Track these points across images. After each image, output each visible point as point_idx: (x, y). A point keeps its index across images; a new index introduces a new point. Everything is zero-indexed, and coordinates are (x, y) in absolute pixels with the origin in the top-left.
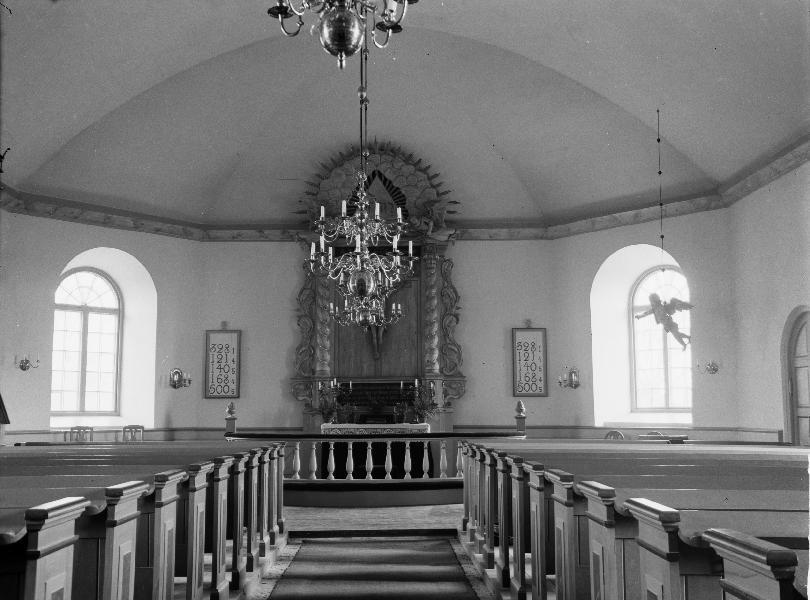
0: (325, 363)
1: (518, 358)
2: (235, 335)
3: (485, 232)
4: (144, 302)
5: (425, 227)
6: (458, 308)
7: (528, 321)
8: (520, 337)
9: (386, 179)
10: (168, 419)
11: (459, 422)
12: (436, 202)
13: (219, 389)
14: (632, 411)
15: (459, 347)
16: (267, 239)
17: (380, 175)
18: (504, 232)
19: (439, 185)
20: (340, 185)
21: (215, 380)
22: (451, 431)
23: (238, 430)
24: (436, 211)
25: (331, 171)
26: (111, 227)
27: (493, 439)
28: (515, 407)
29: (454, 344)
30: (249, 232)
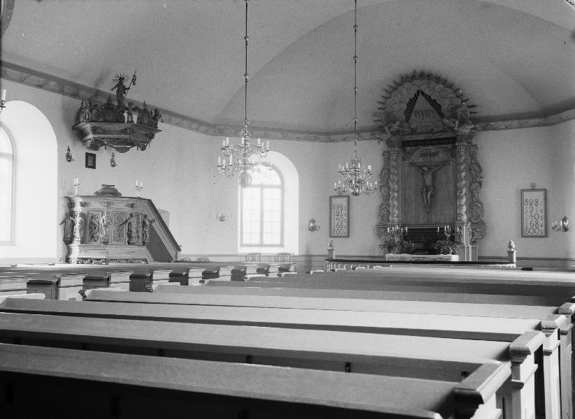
0: (395, 215)
1: (525, 211)
2: (346, 199)
3: (502, 124)
4: (293, 180)
5: (452, 125)
7: (533, 185)
8: (527, 195)
10: (308, 250)
11: (484, 254)
12: (459, 107)
13: (532, 231)
14: (283, 247)
15: (482, 204)
17: (423, 93)
18: (515, 123)
22: (477, 260)
23: (336, 256)
25: (391, 93)
27: (447, 266)
28: (508, 245)
29: (479, 202)
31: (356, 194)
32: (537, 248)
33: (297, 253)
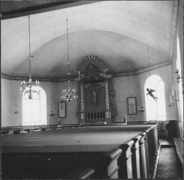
31: (69, 101)
32: (134, 118)
33: (46, 124)
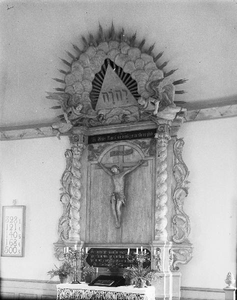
5: (151, 107)
6: (187, 182)
9: (117, 67)
16: (44, 136)
17: (112, 64)
19: (165, 64)
20: (80, 78)
21: (8, 243)
24: (161, 91)
26: (13, 140)
29: (183, 215)
30: (31, 130)
